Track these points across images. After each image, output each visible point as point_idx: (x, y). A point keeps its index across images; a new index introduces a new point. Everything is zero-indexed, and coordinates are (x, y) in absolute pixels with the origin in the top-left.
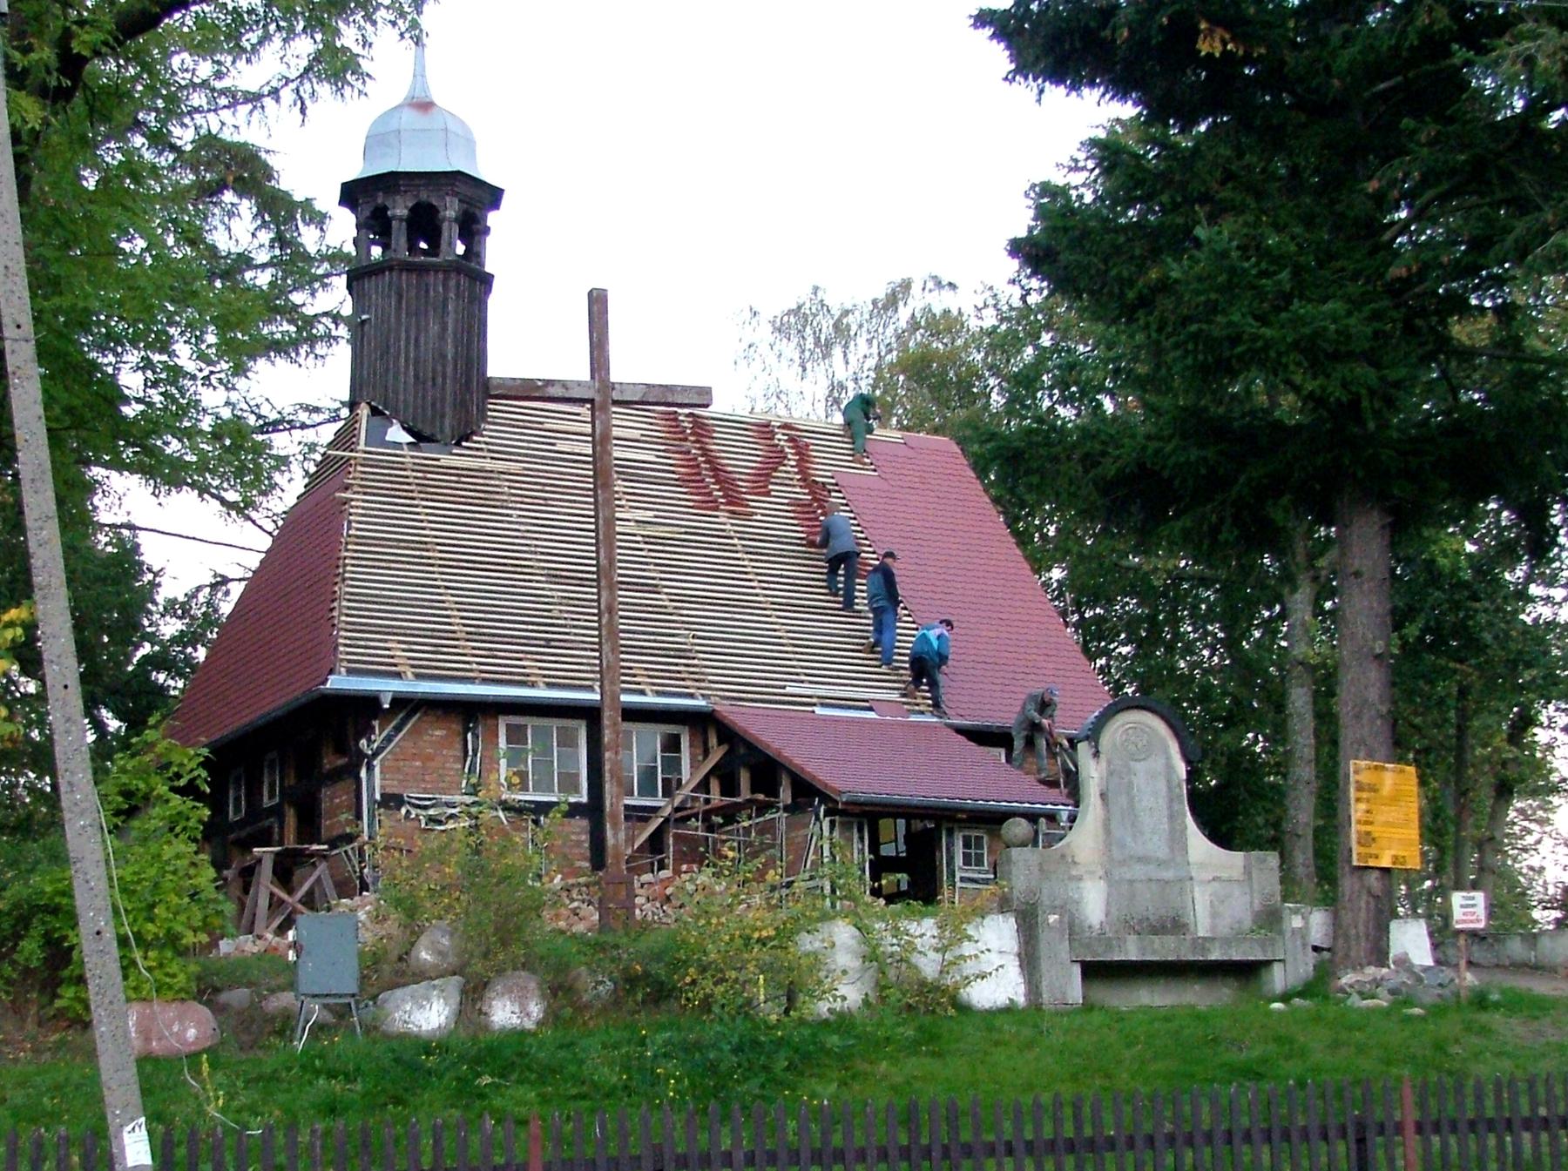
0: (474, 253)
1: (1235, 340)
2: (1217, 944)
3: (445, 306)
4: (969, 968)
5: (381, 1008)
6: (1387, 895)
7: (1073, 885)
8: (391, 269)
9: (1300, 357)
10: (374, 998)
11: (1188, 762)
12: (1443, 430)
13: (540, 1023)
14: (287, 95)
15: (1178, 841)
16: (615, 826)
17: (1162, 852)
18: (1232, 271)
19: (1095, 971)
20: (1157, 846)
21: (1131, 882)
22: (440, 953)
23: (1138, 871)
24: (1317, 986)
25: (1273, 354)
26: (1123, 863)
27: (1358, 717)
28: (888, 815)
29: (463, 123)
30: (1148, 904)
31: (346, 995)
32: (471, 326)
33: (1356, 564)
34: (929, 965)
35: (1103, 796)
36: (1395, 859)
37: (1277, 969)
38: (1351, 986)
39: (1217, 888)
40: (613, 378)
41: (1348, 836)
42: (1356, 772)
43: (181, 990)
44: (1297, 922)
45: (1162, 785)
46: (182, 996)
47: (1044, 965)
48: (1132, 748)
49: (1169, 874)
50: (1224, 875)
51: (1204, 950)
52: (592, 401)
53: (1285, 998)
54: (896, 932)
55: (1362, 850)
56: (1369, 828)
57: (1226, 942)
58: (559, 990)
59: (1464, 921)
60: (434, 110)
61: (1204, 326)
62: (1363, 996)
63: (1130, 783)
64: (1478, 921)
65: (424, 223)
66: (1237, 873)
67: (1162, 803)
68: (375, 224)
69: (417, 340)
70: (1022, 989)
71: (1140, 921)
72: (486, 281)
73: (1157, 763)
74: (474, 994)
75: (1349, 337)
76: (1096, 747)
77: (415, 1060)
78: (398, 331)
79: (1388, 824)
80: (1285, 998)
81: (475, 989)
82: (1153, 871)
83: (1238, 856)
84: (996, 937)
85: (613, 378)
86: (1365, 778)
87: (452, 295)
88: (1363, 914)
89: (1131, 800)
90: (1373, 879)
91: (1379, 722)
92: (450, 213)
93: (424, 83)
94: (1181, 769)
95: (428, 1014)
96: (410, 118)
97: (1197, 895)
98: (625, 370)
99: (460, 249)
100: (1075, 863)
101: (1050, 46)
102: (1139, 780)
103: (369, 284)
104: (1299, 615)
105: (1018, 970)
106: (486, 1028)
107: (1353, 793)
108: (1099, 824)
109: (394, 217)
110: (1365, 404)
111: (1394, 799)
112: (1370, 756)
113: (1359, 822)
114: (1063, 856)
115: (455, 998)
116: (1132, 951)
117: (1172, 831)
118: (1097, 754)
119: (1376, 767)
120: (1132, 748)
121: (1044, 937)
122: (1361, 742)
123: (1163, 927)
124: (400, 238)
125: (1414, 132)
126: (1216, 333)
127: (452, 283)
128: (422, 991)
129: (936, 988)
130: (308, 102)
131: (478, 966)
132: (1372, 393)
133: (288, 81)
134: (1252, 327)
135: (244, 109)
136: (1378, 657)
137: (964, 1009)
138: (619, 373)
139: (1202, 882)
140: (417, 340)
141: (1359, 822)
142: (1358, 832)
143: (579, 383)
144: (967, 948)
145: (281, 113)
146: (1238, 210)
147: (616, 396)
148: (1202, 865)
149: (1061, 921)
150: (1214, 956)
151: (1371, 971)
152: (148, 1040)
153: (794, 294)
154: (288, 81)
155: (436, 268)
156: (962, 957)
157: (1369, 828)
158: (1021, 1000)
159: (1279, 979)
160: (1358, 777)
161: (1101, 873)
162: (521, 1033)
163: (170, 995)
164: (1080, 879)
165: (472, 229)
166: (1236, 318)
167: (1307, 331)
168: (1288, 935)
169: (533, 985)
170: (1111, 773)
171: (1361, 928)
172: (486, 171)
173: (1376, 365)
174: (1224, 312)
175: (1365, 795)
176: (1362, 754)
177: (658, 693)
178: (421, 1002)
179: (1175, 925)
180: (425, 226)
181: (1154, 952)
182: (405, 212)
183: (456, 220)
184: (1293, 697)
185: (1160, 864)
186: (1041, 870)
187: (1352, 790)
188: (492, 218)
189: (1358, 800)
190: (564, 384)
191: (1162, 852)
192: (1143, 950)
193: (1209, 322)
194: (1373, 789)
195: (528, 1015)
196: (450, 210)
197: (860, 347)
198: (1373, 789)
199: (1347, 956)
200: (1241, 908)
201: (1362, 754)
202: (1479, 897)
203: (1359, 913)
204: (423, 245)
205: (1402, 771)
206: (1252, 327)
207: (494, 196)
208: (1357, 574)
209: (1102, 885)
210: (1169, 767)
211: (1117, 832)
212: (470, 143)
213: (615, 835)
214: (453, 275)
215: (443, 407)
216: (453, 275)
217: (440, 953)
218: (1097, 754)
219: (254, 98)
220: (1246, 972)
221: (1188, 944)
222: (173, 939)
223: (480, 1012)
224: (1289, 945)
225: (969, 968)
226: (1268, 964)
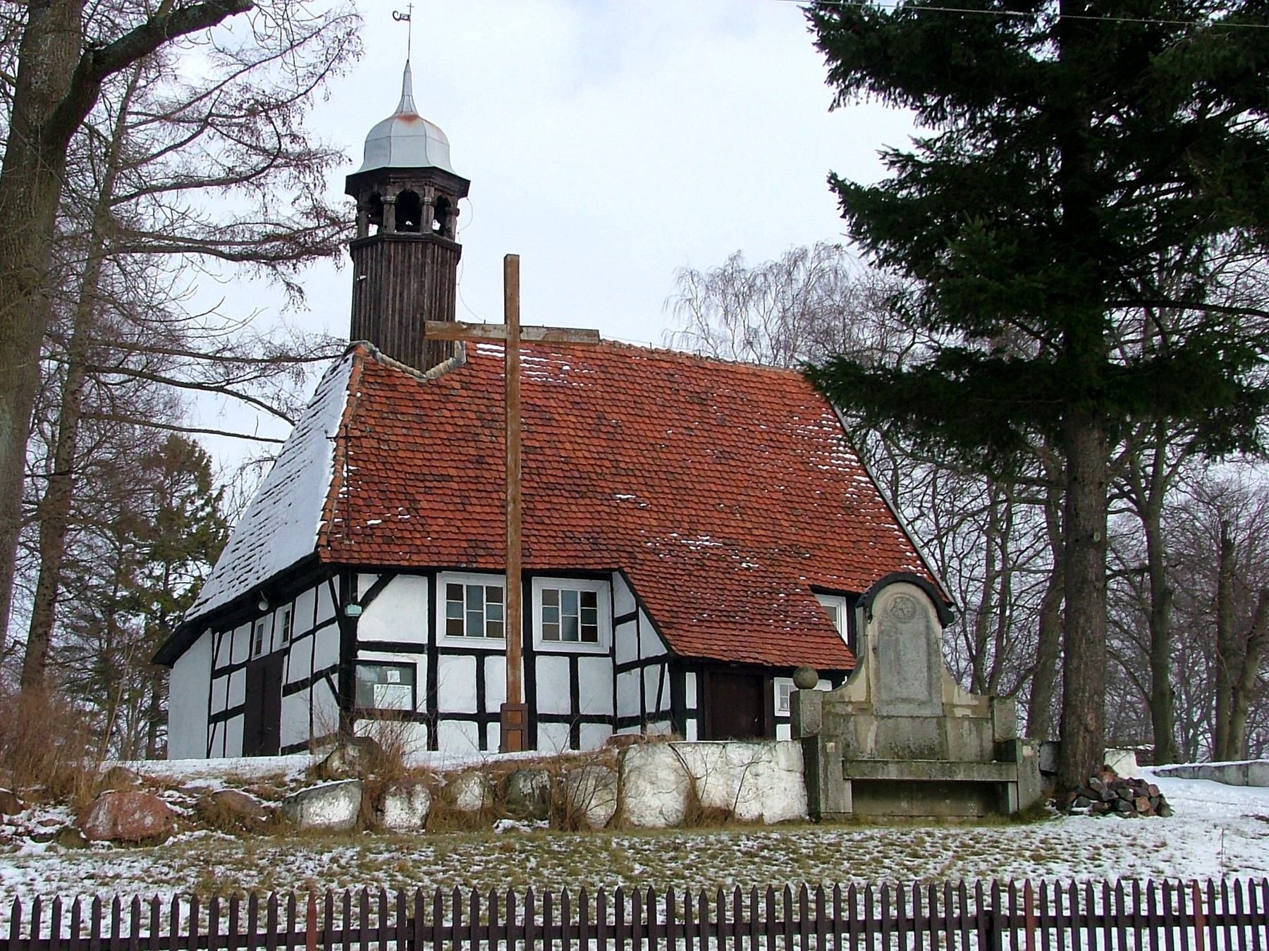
0: (447, 230)
17: (922, 694)
23: (903, 709)
26: (889, 703)
29: (438, 129)
32: (442, 284)
35: (875, 649)
45: (922, 641)
51: (951, 772)
52: (505, 341)
60: (417, 122)
63: (897, 640)
65: (409, 207)
67: (923, 657)
69: (401, 295)
71: (903, 749)
72: (457, 250)
73: (918, 625)
87: (429, 261)
89: (897, 653)
96: (399, 127)
99: (436, 226)
101: (861, 53)
103: (367, 253)
109: (386, 202)
115: (357, 792)
116: (892, 773)
123: (922, 753)
124: (391, 220)
127: (429, 252)
140: (401, 295)
143: (495, 327)
150: (960, 777)
152: (115, 824)
153: (719, 262)
155: (416, 240)
165: (446, 211)
168: (1020, 762)
170: (881, 632)
180: (406, 211)
181: (910, 773)
182: (394, 198)
185: (922, 704)
190: (483, 327)
191: (922, 694)
192: (901, 772)
196: (429, 196)
207: (462, 187)
210: (928, 628)
212: (445, 144)
214: (430, 245)
215: (421, 344)
216: (430, 245)
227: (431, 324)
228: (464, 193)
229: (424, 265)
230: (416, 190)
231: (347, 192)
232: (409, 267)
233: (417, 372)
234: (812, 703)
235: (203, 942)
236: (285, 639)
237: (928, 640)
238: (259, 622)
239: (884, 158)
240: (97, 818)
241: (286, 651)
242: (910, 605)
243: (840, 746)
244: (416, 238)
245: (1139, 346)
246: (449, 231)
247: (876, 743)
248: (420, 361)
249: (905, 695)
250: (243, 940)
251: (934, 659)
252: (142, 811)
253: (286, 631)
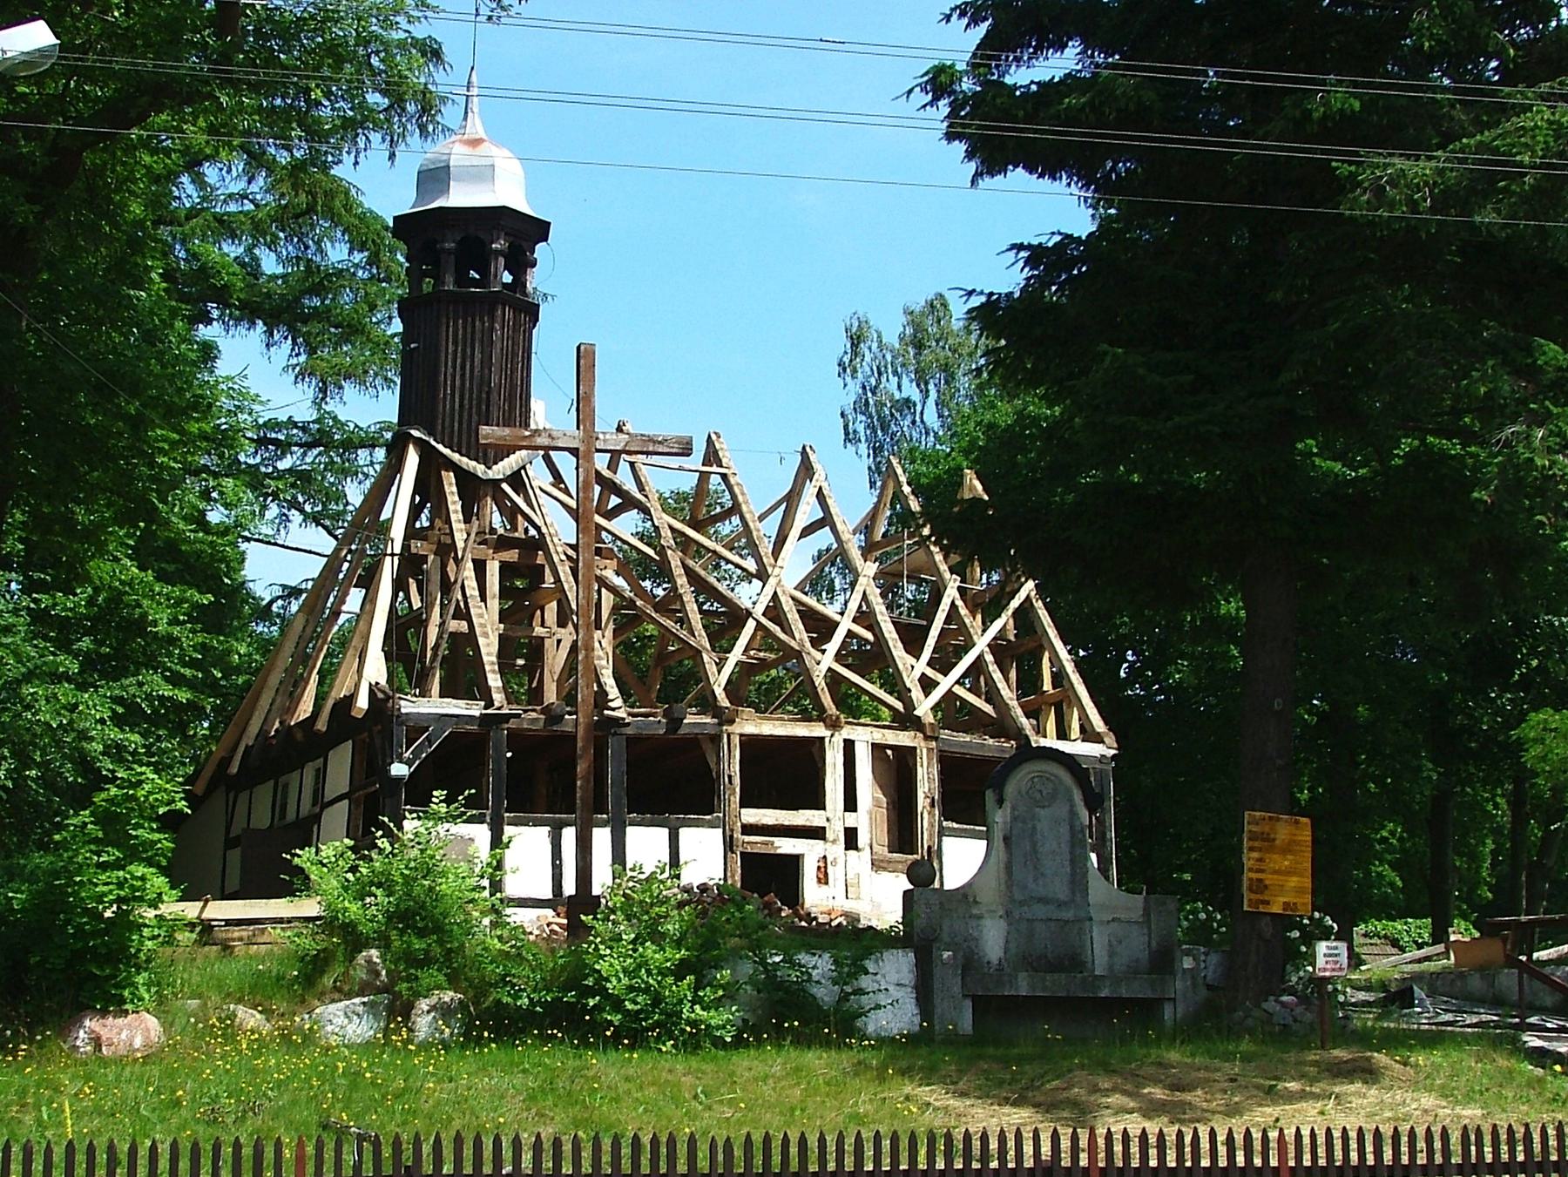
0: (519, 283)
7: (973, 923)
19: (983, 1006)
20: (1060, 890)
23: (1040, 911)
32: (515, 355)
35: (1006, 839)
45: (1064, 830)
49: (1068, 915)
63: (1034, 828)
67: (1065, 848)
73: (1061, 810)
89: (1034, 844)
100: (976, 902)
109: (443, 250)
139: (1102, 923)
164: (980, 917)
165: (521, 262)
170: (1014, 819)
179: (1073, 962)
181: (1045, 989)
185: (1061, 905)
209: (1003, 923)
210: (1073, 814)
227: (485, 430)
228: (544, 237)
229: (492, 329)
231: (395, 218)
234: (928, 905)
235: (1507, 1168)
236: (314, 805)
237: (1072, 827)
238: (282, 780)
241: (317, 819)
242: (1050, 785)
243: (959, 956)
245: (425, 982)
250: (1540, 1167)
251: (1078, 851)
253: (316, 792)
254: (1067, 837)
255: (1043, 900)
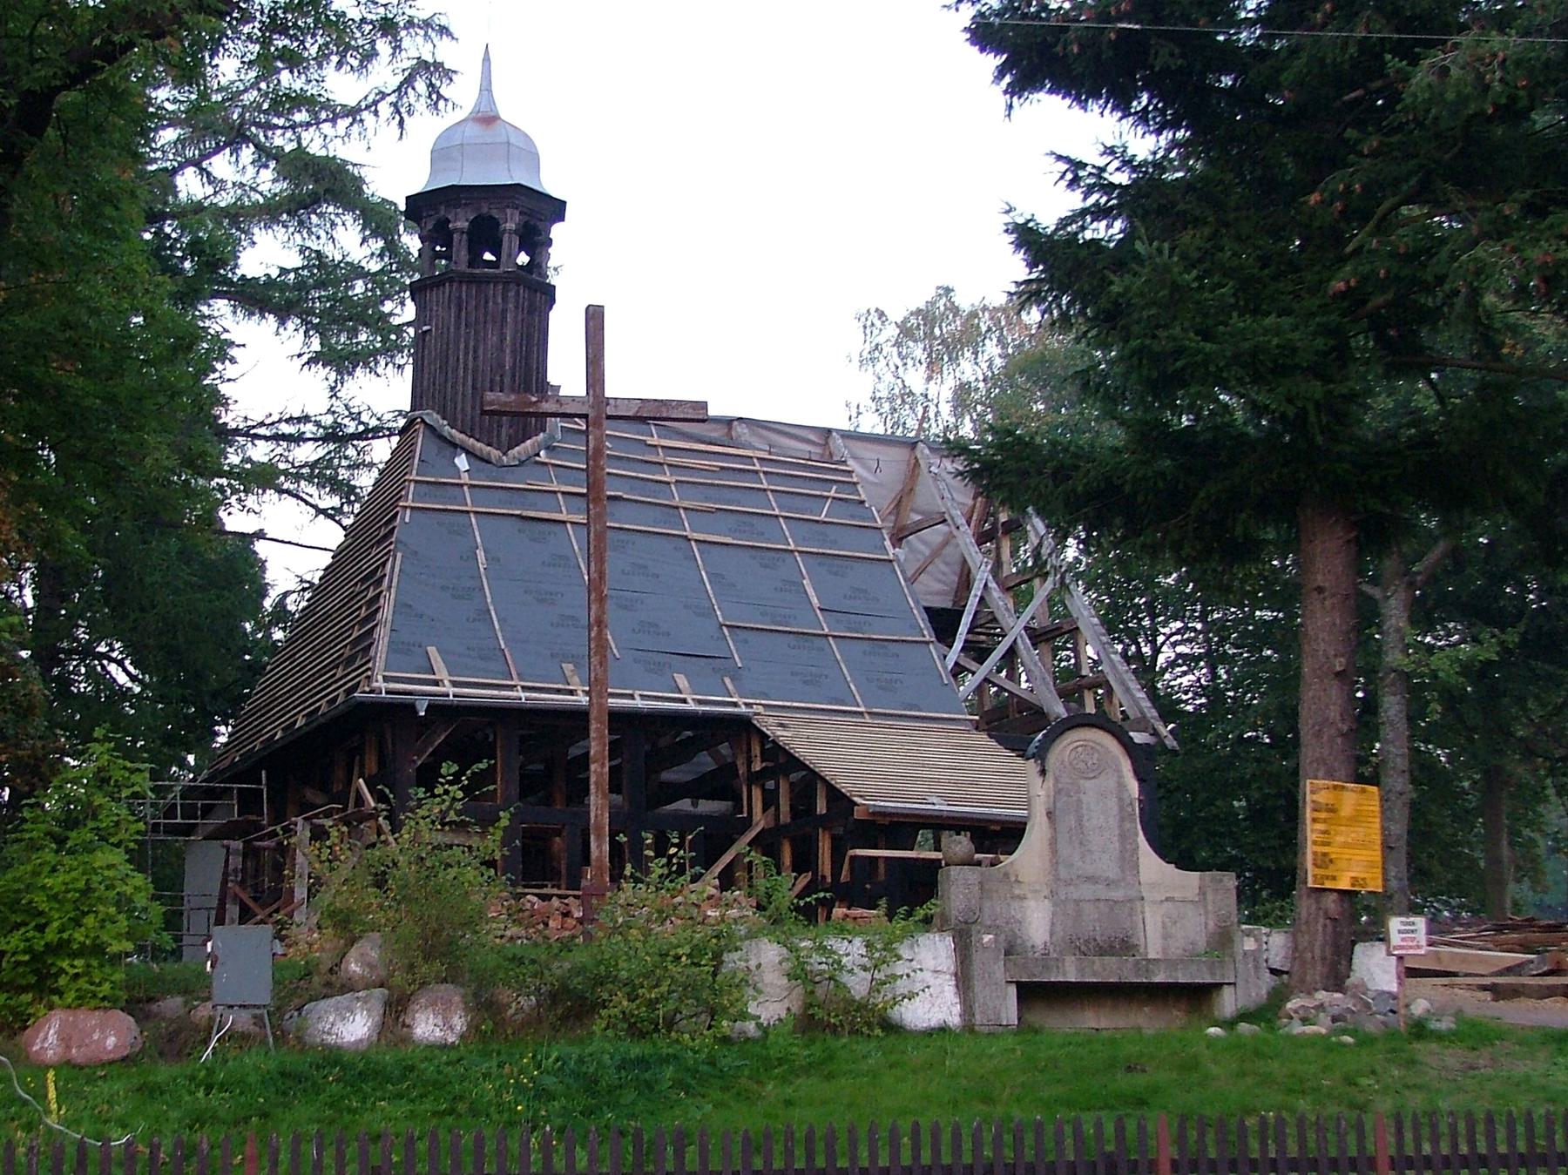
0: (537, 266)
1: (1179, 352)
2: (1163, 967)
3: (504, 318)
4: (902, 986)
5: (305, 1019)
6: (1359, 918)
7: (1015, 904)
8: (451, 281)
9: (1241, 372)
10: (299, 1009)
11: (1140, 780)
12: (1412, 444)
13: (462, 1037)
14: (385, 108)
15: (1129, 862)
16: (599, 837)
18: (1175, 287)
19: (1030, 993)
20: (1107, 866)
21: (1077, 902)
22: (370, 965)
23: (1087, 891)
24: (1267, 1012)
25: (1212, 368)
26: (1068, 883)
27: (1318, 734)
28: (925, 826)
30: (1094, 924)
31: (258, 1007)
33: (1320, 580)
34: (858, 984)
35: (1049, 814)
36: (1355, 880)
37: (1227, 992)
38: (1296, 1012)
39: (1173, 910)
40: (608, 394)
41: (1304, 854)
42: (1313, 792)
43: (104, 999)
44: (1249, 944)
45: (1112, 803)
46: (110, 1002)
47: (978, 985)
48: (1082, 766)
49: (1118, 894)
50: (1177, 895)
52: (584, 416)
53: (1230, 1024)
54: (821, 949)
55: (1317, 871)
56: (1325, 849)
57: (1171, 963)
58: (484, 1007)
59: (1402, 948)
61: (1148, 342)
62: (1305, 1021)
63: (1079, 801)
64: (1419, 947)
66: (1192, 894)
67: (1113, 822)
68: (437, 235)
69: (475, 352)
70: (957, 1009)
71: (1087, 942)
73: (1109, 782)
74: (396, 1009)
75: (1294, 350)
76: (1043, 765)
77: (357, 1073)
78: (457, 343)
79: (1346, 845)
80: (1230, 1024)
81: (399, 1001)
82: (1101, 891)
83: (1194, 877)
84: (931, 956)
85: (608, 394)
86: (1322, 798)
88: (1320, 937)
89: (1080, 820)
90: (1330, 902)
91: (1339, 740)
92: (511, 226)
93: (492, 101)
94: (1133, 787)
95: (353, 1026)
96: (473, 130)
97: (1147, 915)
98: (615, 387)
100: (1017, 881)
101: (1032, 55)
102: (1089, 799)
103: (431, 296)
104: (1393, 621)
105: (953, 989)
106: (407, 1040)
107: (1309, 814)
108: (1046, 843)
109: (456, 230)
110: (1312, 418)
111: (1354, 820)
112: (1330, 775)
113: (1315, 843)
114: (1006, 875)
115: (378, 1009)
116: (1070, 972)
117: (1123, 851)
118: (1043, 772)
119: (1335, 787)
120: (1082, 766)
121: (977, 958)
122: (1321, 761)
123: (1112, 947)
125: (1357, 142)
126: (1157, 347)
127: (512, 294)
128: (346, 1003)
129: (862, 1007)
130: (405, 115)
131: (398, 979)
132: (1318, 406)
133: (383, 95)
134: (1192, 341)
135: (343, 123)
136: (1338, 674)
137: (893, 1028)
138: (615, 387)
141: (1315, 843)
142: (1315, 853)
143: (573, 399)
144: (900, 968)
145: (380, 126)
146: (1197, 222)
147: (610, 411)
148: (1154, 885)
149: (996, 941)
151: (1321, 996)
152: (68, 1047)
154: (383, 95)
155: (495, 280)
156: (895, 977)
157: (1325, 849)
158: (955, 1020)
159: (1228, 1003)
160: (1315, 797)
161: (1046, 892)
162: (444, 1047)
163: (94, 1003)
164: (1022, 898)
165: (536, 241)
166: (1177, 331)
167: (1247, 345)
169: (457, 999)
170: (1058, 792)
171: (1318, 952)
172: (551, 184)
173: (1327, 380)
174: (1166, 327)
175: (1323, 815)
176: (1320, 774)
177: (700, 702)
178: (345, 1013)
179: (1124, 946)
180: (486, 240)
181: (1095, 974)
183: (516, 232)
184: (1386, 706)
185: (1109, 883)
186: (982, 888)
187: (1308, 810)
188: (557, 231)
189: (1314, 820)
192: (1081, 970)
193: (1154, 337)
194: (1331, 809)
195: (451, 1028)
197: (991, 348)
198: (1331, 809)
199: (1302, 981)
200: (1195, 929)
201: (1320, 774)
202: (1420, 923)
203: (1318, 938)
204: (488, 256)
205: (1364, 791)
206: (1192, 341)
207: (557, 209)
208: (1320, 590)
210: (1121, 786)
211: (1064, 850)
213: (600, 846)
217: (370, 965)
218: (1043, 772)
219: (353, 112)
220: (1197, 996)
221: (1129, 966)
222: (97, 949)
223: (404, 1025)
224: (1240, 967)
225: (902, 986)
226: (1218, 986)
227: (489, 396)
229: (504, 311)
230: (495, 214)
232: (486, 315)
233: (498, 453)
237: (1121, 799)
239: (1007, 212)
240: (46, 1038)
244: (496, 276)
246: (539, 266)
247: (1052, 934)
248: (499, 436)
249: (1090, 870)
252: (102, 1031)
254: (1115, 809)
255: (1092, 879)
